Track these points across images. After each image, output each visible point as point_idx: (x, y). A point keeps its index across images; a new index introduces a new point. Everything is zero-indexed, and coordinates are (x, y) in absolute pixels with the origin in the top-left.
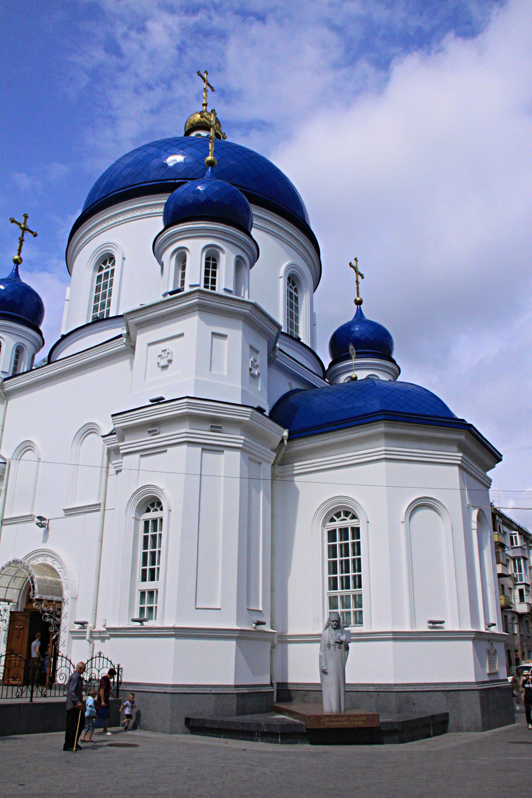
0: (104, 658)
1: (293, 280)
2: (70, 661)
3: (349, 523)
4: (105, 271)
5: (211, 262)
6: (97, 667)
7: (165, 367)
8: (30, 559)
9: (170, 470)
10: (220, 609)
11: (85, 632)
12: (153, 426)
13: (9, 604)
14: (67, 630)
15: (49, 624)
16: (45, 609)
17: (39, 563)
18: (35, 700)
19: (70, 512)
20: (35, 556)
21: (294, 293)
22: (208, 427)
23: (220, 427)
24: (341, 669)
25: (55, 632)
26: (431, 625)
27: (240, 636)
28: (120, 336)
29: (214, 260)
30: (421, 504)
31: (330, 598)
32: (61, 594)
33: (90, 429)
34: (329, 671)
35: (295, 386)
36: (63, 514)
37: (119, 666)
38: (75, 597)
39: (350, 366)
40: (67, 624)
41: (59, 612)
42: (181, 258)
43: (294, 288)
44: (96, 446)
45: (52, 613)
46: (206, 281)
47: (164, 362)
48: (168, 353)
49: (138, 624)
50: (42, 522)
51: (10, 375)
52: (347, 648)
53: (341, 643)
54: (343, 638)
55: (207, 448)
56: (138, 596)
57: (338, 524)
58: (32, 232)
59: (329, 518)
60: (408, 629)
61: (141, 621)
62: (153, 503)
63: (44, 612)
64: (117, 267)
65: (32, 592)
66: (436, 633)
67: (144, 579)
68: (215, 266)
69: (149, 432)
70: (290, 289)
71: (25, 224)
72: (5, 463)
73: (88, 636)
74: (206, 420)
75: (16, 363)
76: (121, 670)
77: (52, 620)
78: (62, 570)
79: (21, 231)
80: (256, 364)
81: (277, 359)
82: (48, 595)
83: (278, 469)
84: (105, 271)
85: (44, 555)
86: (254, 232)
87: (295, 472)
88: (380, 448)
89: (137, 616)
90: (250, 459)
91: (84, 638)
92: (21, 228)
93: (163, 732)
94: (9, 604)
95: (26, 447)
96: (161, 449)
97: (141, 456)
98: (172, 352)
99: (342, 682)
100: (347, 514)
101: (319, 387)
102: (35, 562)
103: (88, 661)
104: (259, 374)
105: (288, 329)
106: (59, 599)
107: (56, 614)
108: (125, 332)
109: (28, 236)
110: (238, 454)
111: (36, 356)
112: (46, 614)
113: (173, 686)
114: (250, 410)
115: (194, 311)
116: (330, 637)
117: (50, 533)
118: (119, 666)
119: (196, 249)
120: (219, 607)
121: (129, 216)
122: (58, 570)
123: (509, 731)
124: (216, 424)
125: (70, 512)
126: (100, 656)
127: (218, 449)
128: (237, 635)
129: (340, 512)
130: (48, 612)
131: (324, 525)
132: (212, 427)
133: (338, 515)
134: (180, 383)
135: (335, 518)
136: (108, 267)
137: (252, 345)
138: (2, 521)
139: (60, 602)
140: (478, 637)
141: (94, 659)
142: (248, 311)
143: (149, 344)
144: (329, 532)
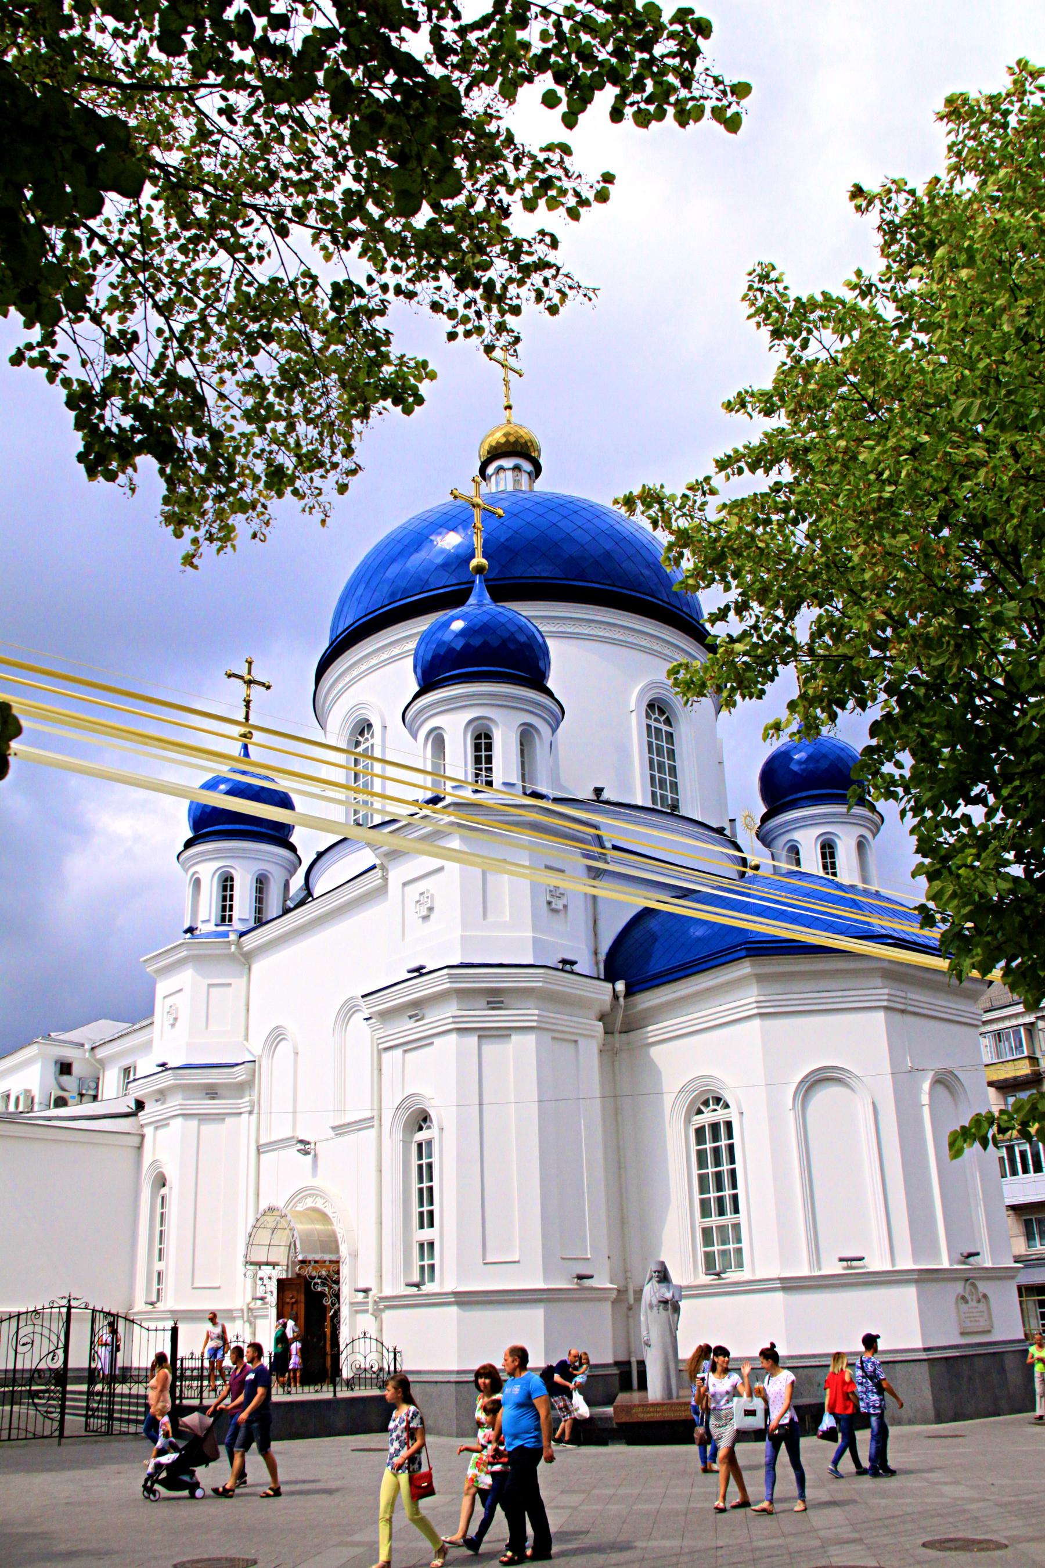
3: (719, 1115)
5: (483, 741)
6: (362, 1351)
7: (426, 918)
15: (322, 1295)
16: (314, 1274)
18: (339, 1395)
19: (340, 1130)
21: (665, 728)
22: (483, 1003)
23: (502, 1002)
24: (668, 1340)
25: (333, 1304)
26: (844, 1263)
28: (374, 867)
30: (816, 1081)
31: (704, 1229)
32: (337, 1250)
34: (652, 1343)
36: (332, 1134)
39: (786, 823)
43: (662, 719)
50: (305, 1146)
51: (252, 924)
52: (676, 1309)
53: (666, 1302)
54: (668, 1295)
57: (707, 1117)
58: (263, 684)
59: (695, 1110)
60: (805, 1272)
62: (422, 1120)
66: (855, 1277)
67: (422, 1227)
68: (489, 747)
69: (410, 1017)
70: (654, 724)
71: (249, 673)
73: (370, 1307)
74: (484, 993)
75: (260, 900)
82: (315, 1252)
85: (310, 1195)
87: (651, 1040)
88: (749, 997)
89: (416, 1278)
91: (366, 1311)
93: (450, 1435)
97: (405, 1051)
99: (671, 1357)
102: (300, 1208)
104: (565, 906)
105: (654, 794)
106: (334, 1258)
109: (256, 691)
111: (291, 882)
113: (459, 1372)
117: (320, 1162)
119: (455, 726)
121: (385, 656)
123: (994, 1422)
124: (495, 998)
125: (340, 1130)
126: (365, 1337)
127: (503, 1034)
131: (688, 1121)
132: (489, 1003)
133: (706, 1103)
134: (443, 944)
136: (367, 740)
139: (338, 1262)
140: (925, 1278)
141: (356, 1342)
143: (404, 884)
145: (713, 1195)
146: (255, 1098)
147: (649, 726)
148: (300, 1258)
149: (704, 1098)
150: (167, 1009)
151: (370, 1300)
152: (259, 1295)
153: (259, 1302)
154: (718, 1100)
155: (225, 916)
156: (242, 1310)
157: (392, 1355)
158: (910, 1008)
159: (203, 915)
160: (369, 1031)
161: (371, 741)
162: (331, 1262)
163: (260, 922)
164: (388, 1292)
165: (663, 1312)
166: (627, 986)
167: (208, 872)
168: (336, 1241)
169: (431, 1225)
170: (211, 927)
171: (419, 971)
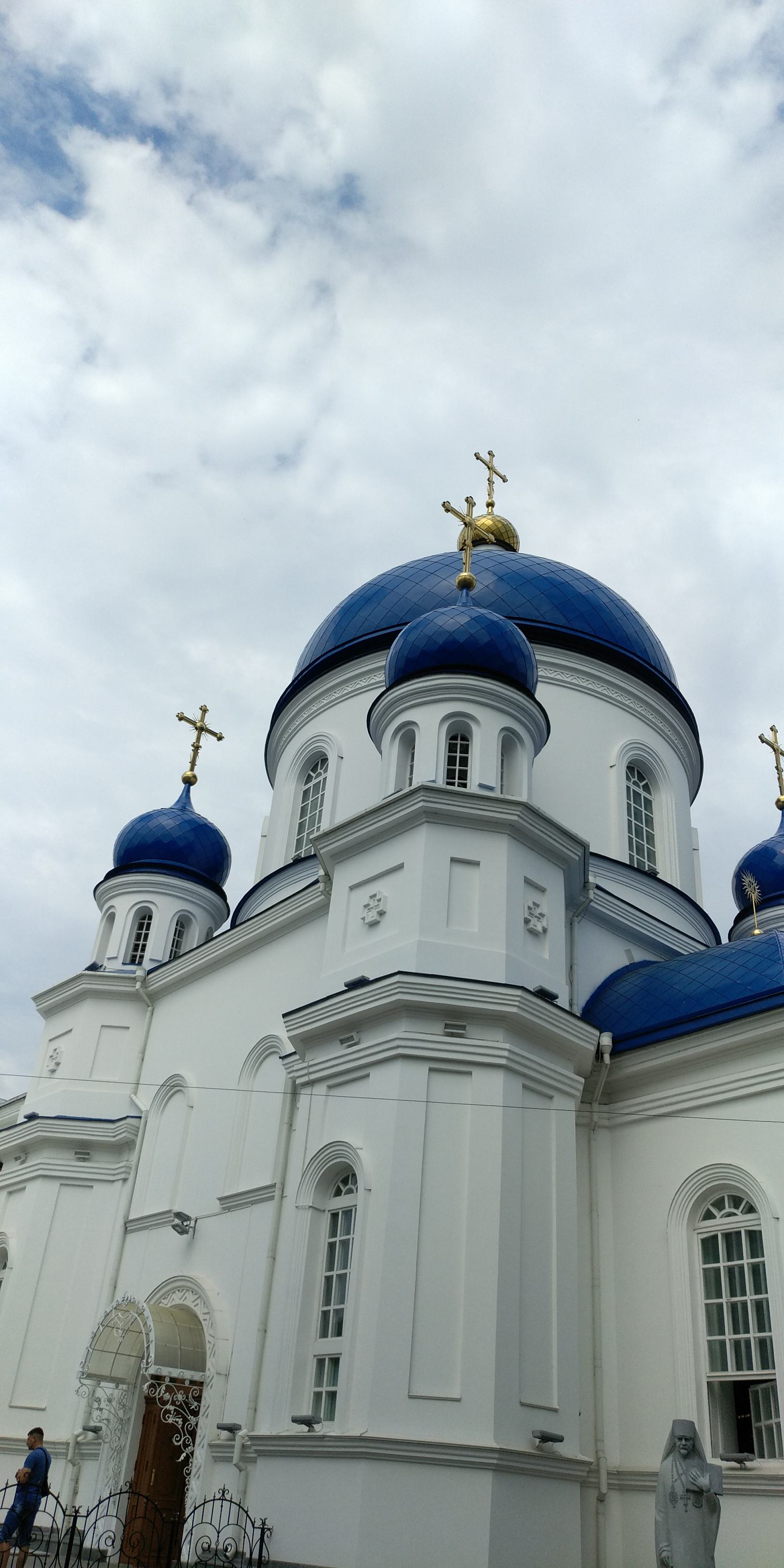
0: (231, 1502)
1: (639, 772)
2: (246, 1512)
3: (740, 1221)
4: (314, 782)
6: (215, 1522)
7: (374, 924)
8: (160, 1298)
9: (373, 1115)
10: (458, 1400)
11: (233, 1447)
12: (348, 1031)
13: (117, 1387)
14: (205, 1442)
16: (167, 1396)
17: (173, 1303)
19: (231, 1203)
20: (170, 1290)
21: (643, 794)
25: (186, 1446)
27: (504, 1464)
28: (316, 882)
29: (464, 738)
32: (202, 1368)
33: (266, 1048)
35: (640, 955)
36: (216, 1206)
37: (264, 1523)
38: (224, 1372)
40: (207, 1429)
41: (196, 1404)
42: (408, 738)
43: (641, 784)
44: (275, 1074)
45: (180, 1406)
46: (450, 774)
47: (372, 916)
48: (379, 900)
49: (305, 1428)
50: (182, 1223)
52: (715, 1509)
55: (441, 1066)
56: (312, 1367)
57: (720, 1224)
59: (702, 1211)
61: (308, 1422)
63: (164, 1403)
64: (330, 774)
65: (145, 1361)
67: (324, 1334)
68: (465, 749)
69: (342, 1042)
70: (633, 787)
71: (202, 720)
72: (140, 1117)
73: (236, 1454)
74: (439, 1015)
76: (268, 1533)
77: (180, 1421)
78: (207, 1317)
79: (196, 733)
80: (537, 912)
81: (592, 904)
83: (599, 1113)
84: (314, 782)
85: (179, 1289)
86: (542, 693)
89: (306, 1411)
90: (525, 1087)
91: (229, 1460)
92: (196, 728)
94: (117, 1387)
95: (173, 1087)
96: (356, 1075)
98: (385, 897)
100: (736, 1201)
101: (685, 953)
103: (100, 1502)
104: (545, 930)
106: (197, 1376)
107: (188, 1408)
108: (321, 872)
109: (206, 739)
110: (497, 1079)
112: (168, 1407)
114: (519, 992)
115: (420, 825)
116: (676, 1476)
118: (264, 1523)
119: (430, 723)
120: (457, 1396)
122: (201, 1317)
124: (456, 1020)
128: (495, 1462)
129: (723, 1199)
130: (173, 1403)
133: (719, 1204)
135: (714, 1211)
136: (320, 774)
137: (528, 876)
138: (125, 1224)
139: (201, 1384)
141: (209, 1506)
142: (515, 818)
144: (704, 1242)
145: (729, 1336)
146: (133, 1163)
147: (628, 788)
148: (152, 1370)
149: (717, 1196)
150: (51, 1053)
151: (238, 1443)
152: (92, 1424)
153: (91, 1434)
154: (736, 1201)
155: (135, 959)
156: (68, 1444)
157: (258, 1532)
158: (313, 1077)
159: (111, 952)
160: (285, 1072)
161: (323, 776)
162: (192, 1382)
163: (175, 956)
164: (263, 1430)
165: (693, 1512)
166: (614, 1040)
167: (125, 907)
168: (204, 1354)
169: (339, 1333)
170: (117, 965)
171: (362, 982)
